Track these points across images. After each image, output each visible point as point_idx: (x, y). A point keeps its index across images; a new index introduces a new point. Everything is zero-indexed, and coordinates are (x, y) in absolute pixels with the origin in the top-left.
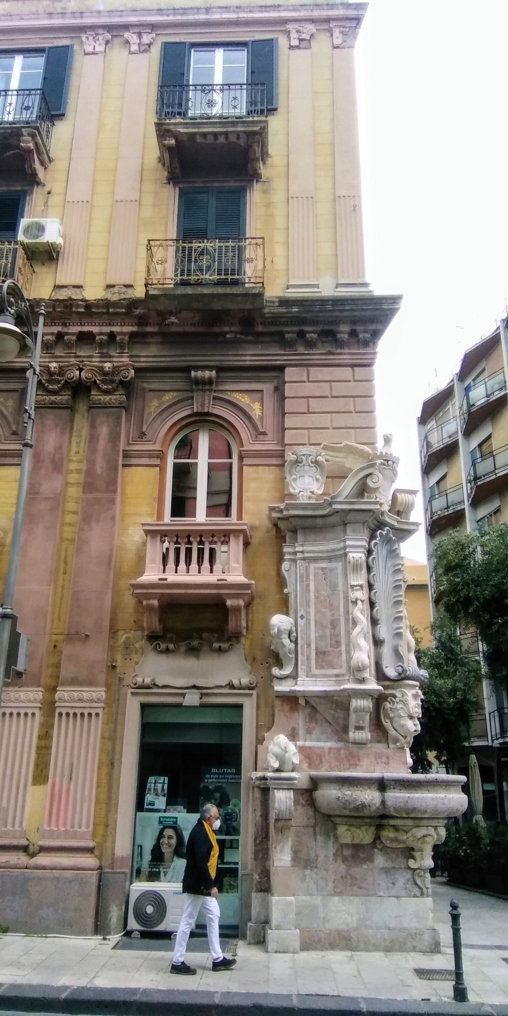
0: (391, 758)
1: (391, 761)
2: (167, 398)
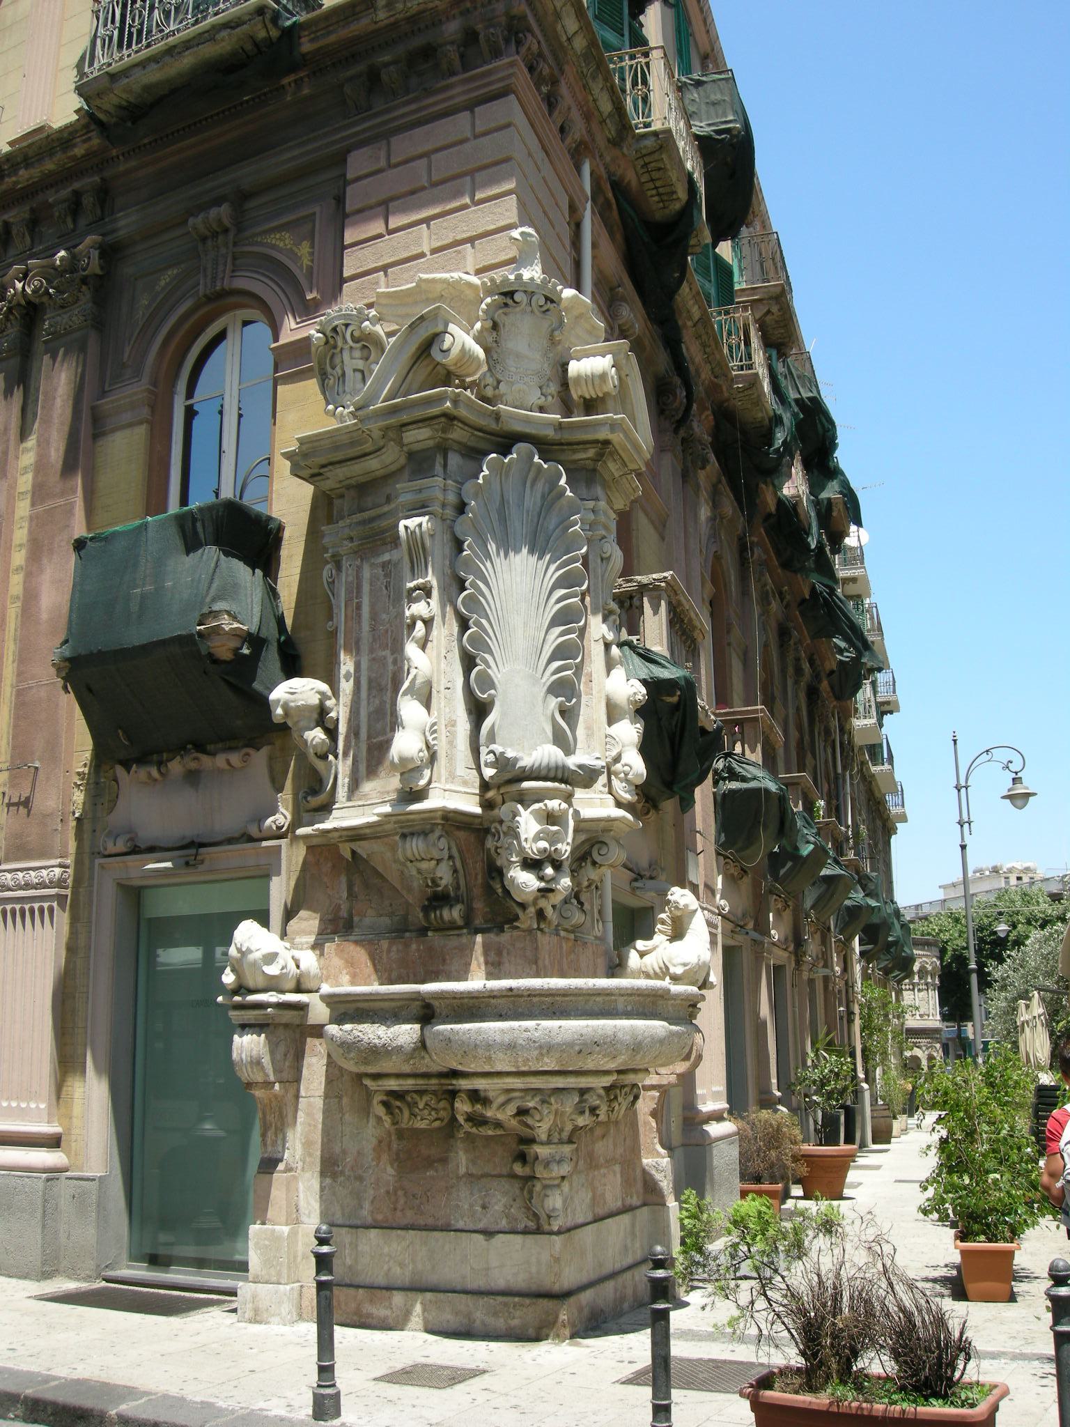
0: (505, 953)
1: (505, 958)
2: (162, 283)
